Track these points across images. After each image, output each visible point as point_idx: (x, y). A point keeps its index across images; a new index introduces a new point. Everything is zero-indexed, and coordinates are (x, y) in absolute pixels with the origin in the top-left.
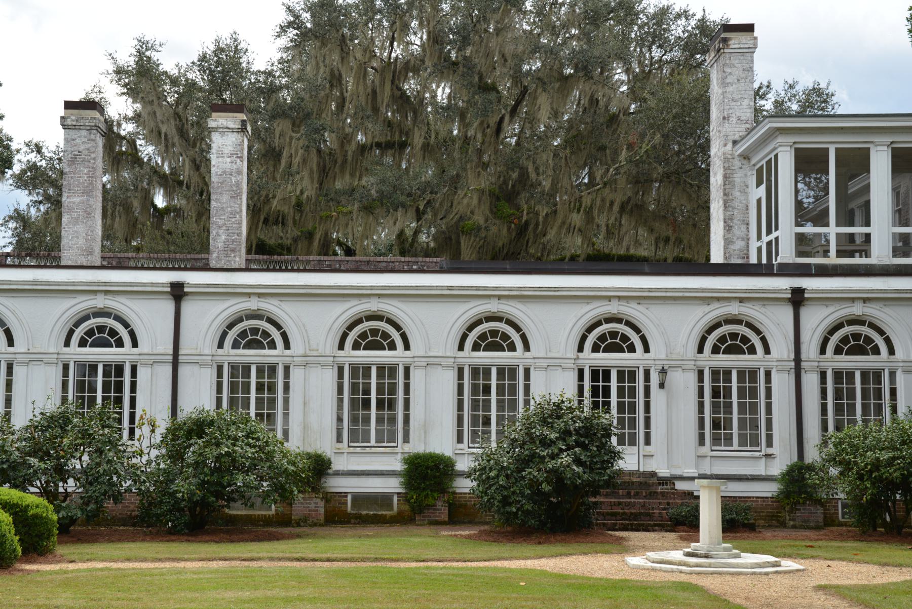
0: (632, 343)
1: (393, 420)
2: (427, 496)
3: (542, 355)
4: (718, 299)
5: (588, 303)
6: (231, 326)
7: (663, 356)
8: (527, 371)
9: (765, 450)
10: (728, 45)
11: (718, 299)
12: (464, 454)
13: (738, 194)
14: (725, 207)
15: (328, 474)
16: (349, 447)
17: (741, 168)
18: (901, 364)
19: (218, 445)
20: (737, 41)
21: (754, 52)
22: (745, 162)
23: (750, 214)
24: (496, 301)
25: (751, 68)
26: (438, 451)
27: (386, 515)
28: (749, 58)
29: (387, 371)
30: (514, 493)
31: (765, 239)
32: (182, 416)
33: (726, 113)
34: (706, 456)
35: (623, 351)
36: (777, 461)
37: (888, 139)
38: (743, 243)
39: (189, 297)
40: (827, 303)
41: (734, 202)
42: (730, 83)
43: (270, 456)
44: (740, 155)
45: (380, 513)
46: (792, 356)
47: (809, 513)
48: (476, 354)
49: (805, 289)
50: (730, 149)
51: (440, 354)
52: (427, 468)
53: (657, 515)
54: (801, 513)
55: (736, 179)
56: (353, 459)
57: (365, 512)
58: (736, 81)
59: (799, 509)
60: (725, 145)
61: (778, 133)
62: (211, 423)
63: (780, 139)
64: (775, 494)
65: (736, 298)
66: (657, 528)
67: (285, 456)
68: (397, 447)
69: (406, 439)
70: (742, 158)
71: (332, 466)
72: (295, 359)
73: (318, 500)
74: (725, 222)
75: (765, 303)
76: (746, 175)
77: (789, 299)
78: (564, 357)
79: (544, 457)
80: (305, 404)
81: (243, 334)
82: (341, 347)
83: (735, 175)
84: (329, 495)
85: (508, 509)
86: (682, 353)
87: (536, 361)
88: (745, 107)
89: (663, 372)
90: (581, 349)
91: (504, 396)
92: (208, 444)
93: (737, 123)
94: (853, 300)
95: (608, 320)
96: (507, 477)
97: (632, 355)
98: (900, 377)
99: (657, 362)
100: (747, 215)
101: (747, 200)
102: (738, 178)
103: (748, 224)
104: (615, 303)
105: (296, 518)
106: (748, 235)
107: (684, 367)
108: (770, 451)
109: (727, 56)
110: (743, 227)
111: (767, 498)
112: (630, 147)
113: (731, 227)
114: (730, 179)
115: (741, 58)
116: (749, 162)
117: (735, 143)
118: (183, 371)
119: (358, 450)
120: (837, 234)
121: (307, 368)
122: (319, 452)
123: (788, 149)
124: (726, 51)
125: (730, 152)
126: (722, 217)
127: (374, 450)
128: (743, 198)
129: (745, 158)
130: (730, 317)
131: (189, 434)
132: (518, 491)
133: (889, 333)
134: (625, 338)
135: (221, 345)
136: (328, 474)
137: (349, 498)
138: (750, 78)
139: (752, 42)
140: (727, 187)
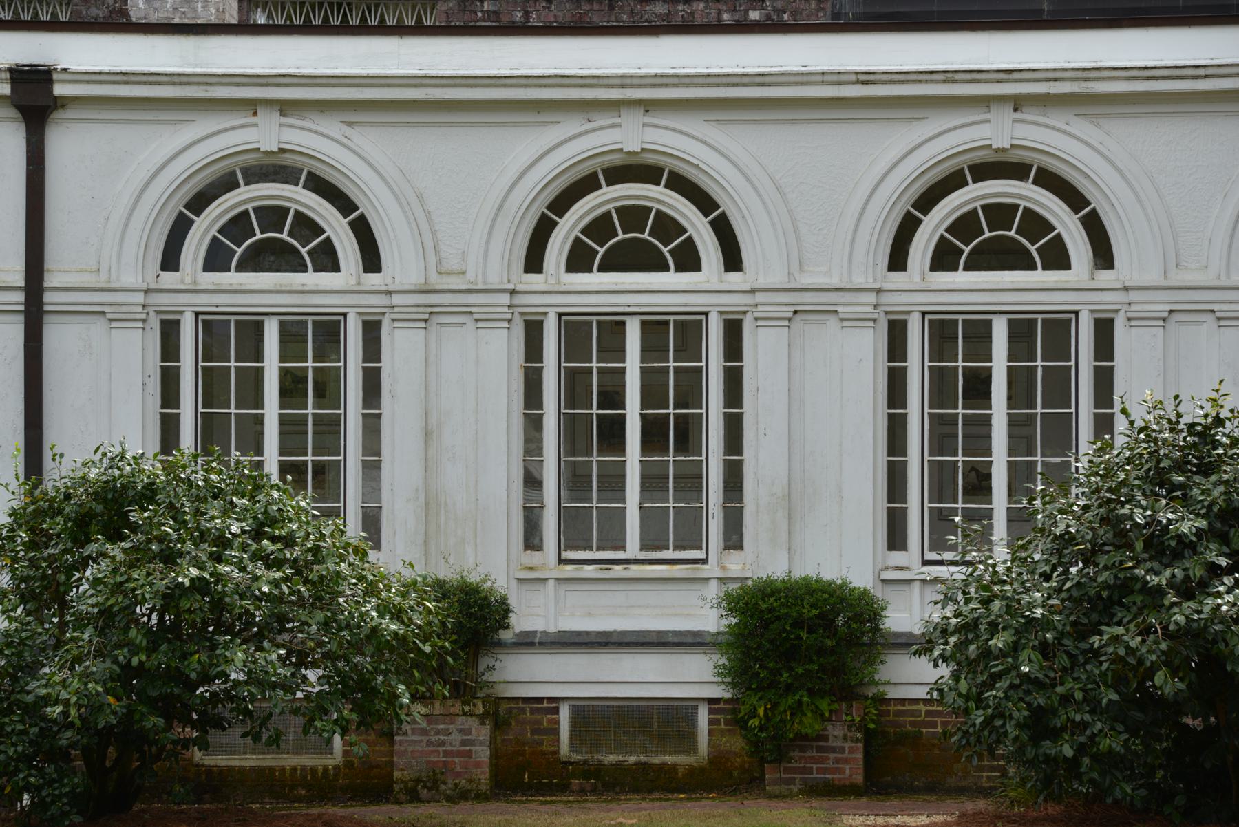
1: (692, 482)
2: (798, 709)
6: (199, 202)
8: (1104, 330)
15: (501, 644)
16: (561, 561)
19: (170, 558)
24: (1007, 114)
26: (830, 572)
27: (674, 767)
30: (1066, 699)
32: (57, 475)
39: (69, 114)
43: (325, 592)
45: (657, 760)
48: (945, 279)
51: (835, 282)
52: (798, 624)
56: (576, 598)
57: (611, 758)
62: (149, 494)
65: (1001, 99)
67: (371, 590)
69: (734, 540)
71: (513, 619)
72: (397, 300)
73: (472, 723)
78: (1224, 282)
79: (1159, 591)
80: (427, 434)
82: (534, 262)
84: (503, 707)
85: (1048, 747)
87: (1133, 296)
89: (372, 331)
92: (138, 557)
96: (1045, 650)
105: (407, 775)
118: (56, 336)
119: (589, 572)
121: (434, 329)
122: (473, 578)
127: (635, 571)
131: (82, 528)
135: (170, 261)
136: (501, 644)
137: (564, 714)
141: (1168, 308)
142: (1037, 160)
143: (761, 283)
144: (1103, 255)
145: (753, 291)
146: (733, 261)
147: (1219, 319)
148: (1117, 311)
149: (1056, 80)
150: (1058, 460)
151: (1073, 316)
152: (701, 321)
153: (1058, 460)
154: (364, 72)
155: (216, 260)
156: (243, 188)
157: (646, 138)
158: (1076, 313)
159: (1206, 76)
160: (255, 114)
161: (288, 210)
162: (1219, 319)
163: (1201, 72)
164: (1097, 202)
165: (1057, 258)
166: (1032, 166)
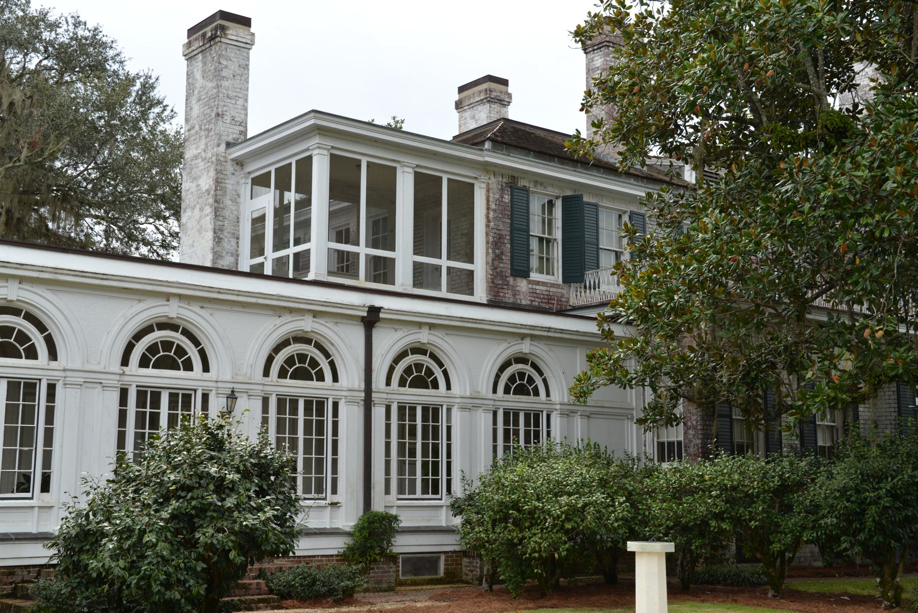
0: (189, 358)
3: (77, 366)
4: (291, 310)
5: (140, 301)
7: (228, 377)
8: (52, 388)
9: (330, 498)
10: (225, 34)
11: (291, 310)
12: (33, 507)
13: (229, 202)
14: (216, 216)
17: (233, 174)
18: (458, 400)
20: (234, 32)
21: (250, 49)
22: (238, 168)
23: (240, 227)
25: (247, 65)
28: (245, 54)
29: (432, 413)
31: (292, 250)
33: (220, 109)
34: (392, 507)
35: (427, 387)
36: (342, 511)
37: (415, 162)
38: (232, 259)
40: (396, 327)
41: (225, 211)
42: (225, 77)
44: (233, 160)
46: (363, 386)
47: (382, 572)
48: (144, 371)
49: (381, 308)
50: (223, 151)
53: (254, 587)
54: (375, 573)
55: (228, 186)
58: (231, 76)
59: (373, 569)
60: (218, 145)
61: (316, 132)
63: (316, 140)
64: (342, 551)
65: (309, 311)
66: (261, 605)
68: (32, 498)
70: (234, 163)
74: (215, 233)
75: (338, 321)
76: (238, 183)
77: (363, 319)
78: (107, 370)
81: (153, 349)
83: (227, 181)
86: (248, 375)
87: (68, 374)
88: (240, 107)
89: (548, 417)
90: (125, 362)
91: (17, 423)
93: (231, 123)
94: (420, 325)
95: (162, 326)
97: (188, 374)
98: (456, 413)
99: (220, 385)
100: (237, 229)
101: (238, 211)
102: (230, 184)
103: (238, 238)
104: (175, 303)
106: (237, 251)
107: (251, 393)
108: (335, 498)
109: (224, 46)
110: (233, 241)
111: (332, 556)
112: (32, 145)
113: (221, 239)
114: (222, 185)
115: (238, 52)
116: (242, 169)
117: (229, 145)
120: (394, 251)
123: (325, 152)
124: (223, 40)
125: (223, 155)
126: (210, 227)
128: (234, 208)
129: (237, 164)
130: (300, 334)
132: (182, 565)
133: (448, 365)
134: (181, 351)
137: (443, 557)
138: (245, 76)
139: (249, 37)
140: (219, 193)
141: (83, 380)
142: (26, 308)
143: (70, 366)
144: (53, 354)
145: (64, 370)
146: (206, 368)
147: (103, 387)
148: (58, 380)
149: (42, 271)
150: (27, 449)
151: (38, 381)
152: (191, 395)
153: (27, 449)
154: (257, 291)
155: (282, 374)
156: (410, 356)
157: (19, 295)
158: (40, 380)
159: (107, 279)
160: (168, 300)
161: (174, 343)
162: (103, 387)
163: (105, 277)
164: (52, 329)
165: (32, 353)
166: (22, 311)
